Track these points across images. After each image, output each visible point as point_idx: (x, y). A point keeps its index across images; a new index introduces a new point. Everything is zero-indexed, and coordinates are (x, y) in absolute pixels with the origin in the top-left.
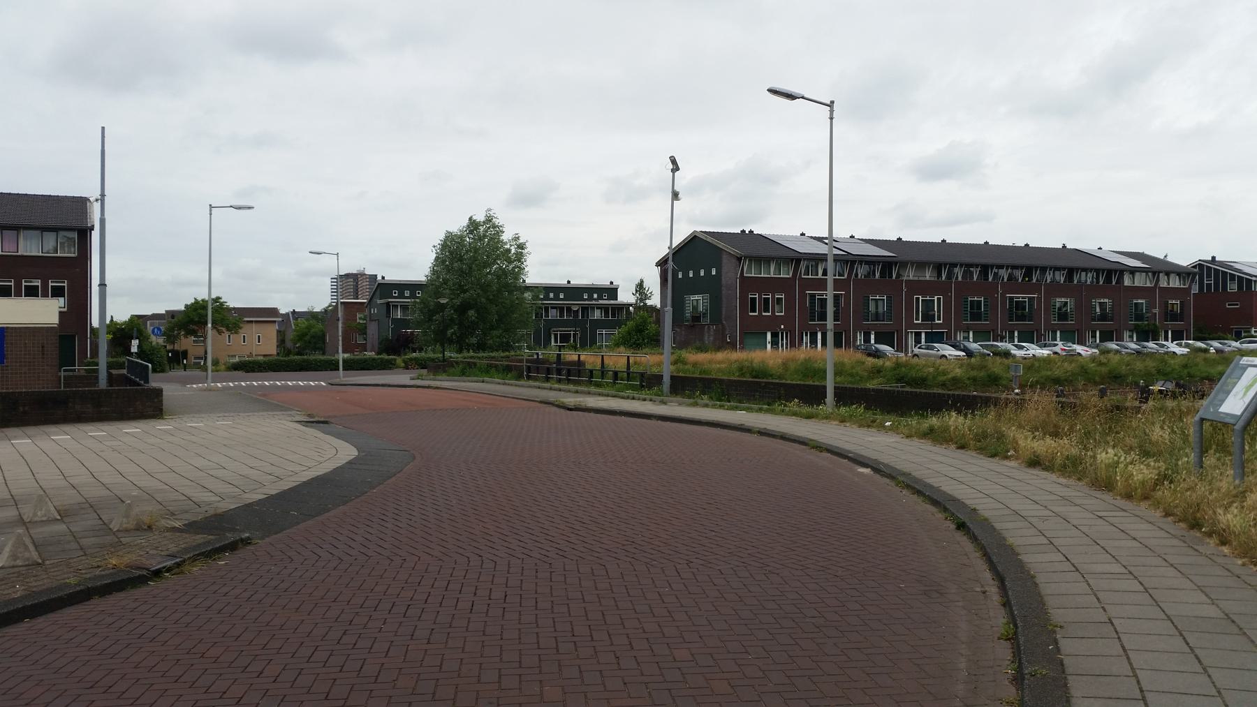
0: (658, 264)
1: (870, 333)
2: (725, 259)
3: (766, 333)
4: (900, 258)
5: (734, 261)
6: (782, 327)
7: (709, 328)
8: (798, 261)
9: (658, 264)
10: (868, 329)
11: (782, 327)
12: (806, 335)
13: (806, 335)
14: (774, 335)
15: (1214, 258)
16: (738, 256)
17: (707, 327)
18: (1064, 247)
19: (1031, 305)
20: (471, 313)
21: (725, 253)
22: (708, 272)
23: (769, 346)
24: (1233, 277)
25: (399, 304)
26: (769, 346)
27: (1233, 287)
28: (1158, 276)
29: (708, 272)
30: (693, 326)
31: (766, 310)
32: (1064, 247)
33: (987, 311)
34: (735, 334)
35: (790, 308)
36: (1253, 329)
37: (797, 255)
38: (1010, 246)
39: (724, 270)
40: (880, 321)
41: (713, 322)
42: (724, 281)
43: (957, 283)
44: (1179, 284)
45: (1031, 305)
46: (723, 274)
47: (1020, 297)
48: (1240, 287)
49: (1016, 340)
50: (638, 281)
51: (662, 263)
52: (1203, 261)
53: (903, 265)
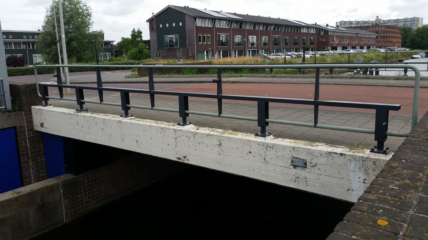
0: (148, 21)
1: (284, 49)
2: (187, 18)
3: (204, 51)
4: (245, 20)
5: (192, 19)
6: (210, 49)
7: (179, 50)
8: (215, 19)
9: (148, 21)
10: (236, 49)
11: (210, 49)
12: (217, 52)
13: (217, 52)
14: (207, 52)
15: (316, 23)
16: (195, 16)
17: (178, 49)
18: (279, 18)
19: (279, 39)
20: (74, 43)
21: (187, 15)
22: (177, 24)
23: (205, 57)
24: (322, 29)
25: (22, 42)
26: (205, 57)
27: (322, 33)
28: (301, 29)
29: (177, 24)
30: (169, 49)
31: (204, 41)
32: (279, 18)
33: (226, 44)
34: (194, 52)
35: (212, 41)
36: (328, 47)
37: (214, 17)
38: (266, 17)
39: (187, 23)
40: (239, 46)
41: (181, 47)
42: (187, 28)
43: (261, 30)
44: (313, 32)
45: (279, 39)
46: (187, 26)
47: (276, 36)
48: (325, 33)
49: (275, 53)
50: (132, 30)
51: (150, 21)
52: (313, 24)
53: (246, 22)
